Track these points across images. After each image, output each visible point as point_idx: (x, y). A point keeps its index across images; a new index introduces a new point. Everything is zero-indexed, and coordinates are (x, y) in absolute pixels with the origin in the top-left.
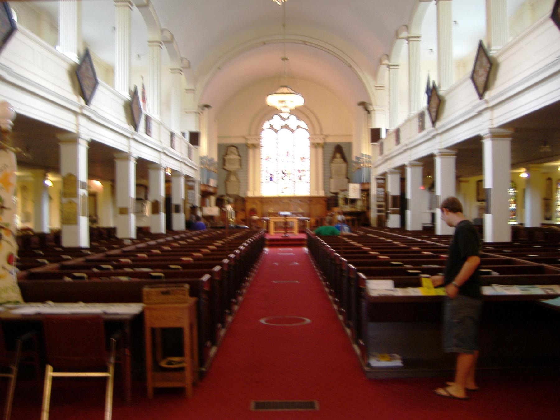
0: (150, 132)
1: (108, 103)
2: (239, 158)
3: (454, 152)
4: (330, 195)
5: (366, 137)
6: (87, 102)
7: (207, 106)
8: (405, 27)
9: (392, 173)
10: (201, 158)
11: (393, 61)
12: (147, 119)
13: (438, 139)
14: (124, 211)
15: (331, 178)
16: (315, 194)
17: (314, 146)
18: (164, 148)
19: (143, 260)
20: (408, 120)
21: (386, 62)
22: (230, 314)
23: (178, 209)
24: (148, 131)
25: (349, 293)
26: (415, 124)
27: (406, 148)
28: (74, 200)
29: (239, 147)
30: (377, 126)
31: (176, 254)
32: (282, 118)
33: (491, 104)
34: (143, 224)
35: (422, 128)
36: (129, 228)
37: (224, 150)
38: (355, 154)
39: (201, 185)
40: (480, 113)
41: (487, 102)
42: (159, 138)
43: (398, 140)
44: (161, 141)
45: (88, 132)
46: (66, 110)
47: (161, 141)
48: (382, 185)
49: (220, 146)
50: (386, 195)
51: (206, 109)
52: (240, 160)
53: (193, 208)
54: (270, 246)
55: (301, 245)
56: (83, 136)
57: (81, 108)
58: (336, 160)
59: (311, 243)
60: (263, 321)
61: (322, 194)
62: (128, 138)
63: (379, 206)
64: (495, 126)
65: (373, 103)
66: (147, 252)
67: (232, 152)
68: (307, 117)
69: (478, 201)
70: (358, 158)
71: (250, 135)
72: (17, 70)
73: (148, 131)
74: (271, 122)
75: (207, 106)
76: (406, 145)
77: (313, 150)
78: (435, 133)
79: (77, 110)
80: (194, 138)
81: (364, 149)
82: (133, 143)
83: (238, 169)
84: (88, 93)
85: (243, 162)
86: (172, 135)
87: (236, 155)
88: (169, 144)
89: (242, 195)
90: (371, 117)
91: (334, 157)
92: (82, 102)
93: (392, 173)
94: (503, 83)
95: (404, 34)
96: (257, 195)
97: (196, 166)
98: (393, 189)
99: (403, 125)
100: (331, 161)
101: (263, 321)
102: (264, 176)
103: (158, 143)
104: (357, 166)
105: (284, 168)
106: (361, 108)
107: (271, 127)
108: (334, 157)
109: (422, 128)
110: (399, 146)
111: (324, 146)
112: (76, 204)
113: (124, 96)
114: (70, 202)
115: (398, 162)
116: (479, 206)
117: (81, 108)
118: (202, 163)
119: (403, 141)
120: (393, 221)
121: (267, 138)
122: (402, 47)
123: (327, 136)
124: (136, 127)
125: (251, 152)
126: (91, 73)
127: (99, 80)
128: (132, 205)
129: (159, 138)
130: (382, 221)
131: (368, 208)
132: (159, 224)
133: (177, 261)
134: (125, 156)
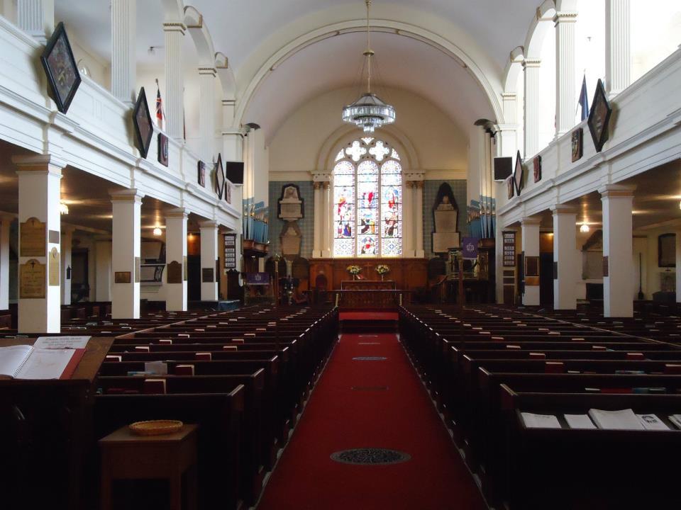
0: (166, 160)
1: (97, 112)
2: (300, 202)
3: (633, 188)
4: (432, 256)
5: (488, 170)
6: (63, 108)
7: (255, 126)
8: (521, 49)
9: (528, 223)
10: (245, 202)
11: (531, 55)
12: (161, 139)
13: (605, 169)
14: (123, 278)
15: (435, 232)
16: (411, 255)
17: (410, 185)
18: (187, 185)
19: (166, 347)
20: (556, 143)
21: (520, 58)
22: (281, 445)
23: (208, 276)
24: (162, 158)
25: (487, 424)
26: (568, 148)
27: (551, 185)
28: (40, 259)
29: (301, 187)
30: (505, 155)
31: (213, 340)
32: (363, 144)
33: (608, 158)
34: (152, 297)
35: (578, 153)
36: (131, 302)
37: (278, 190)
38: (471, 197)
39: (243, 241)
40: (598, 167)
41: (604, 155)
42: (181, 167)
43: (538, 175)
44: (183, 175)
45: (63, 154)
46: (7, 110)
47: (183, 175)
48: (513, 244)
49: (273, 185)
50: (520, 257)
51: (253, 130)
52: (302, 205)
53: (233, 275)
54: (345, 331)
55: (393, 331)
56: (139, 192)
57: (52, 115)
58: (441, 205)
59: (406, 327)
60: (335, 456)
61: (421, 254)
62: (131, 167)
63: (506, 273)
64: (561, 203)
65: (499, 120)
66: (172, 336)
67: (291, 194)
68: (401, 143)
69: (660, 265)
70: (473, 202)
71: (316, 169)
72: (84, 125)
73: (162, 158)
74: (349, 151)
75: (255, 126)
76: (552, 181)
77: (409, 191)
78: (601, 160)
79: (46, 119)
80: (235, 172)
81: (486, 189)
82: (137, 174)
83: (299, 218)
84: (64, 94)
85: (306, 208)
86: (200, 165)
87: (296, 200)
88: (196, 179)
89: (305, 255)
90: (495, 142)
91: (439, 201)
92: (138, 155)
93: (528, 223)
94: (624, 132)
95: (520, 58)
96: (325, 256)
97: (236, 212)
98: (529, 245)
99: (547, 151)
100: (434, 209)
101: (335, 456)
102: (339, 217)
103: (180, 177)
104: (474, 214)
105: (366, 213)
106: (480, 129)
107: (349, 158)
108: (439, 201)
109: (578, 153)
110: (540, 183)
111: (423, 185)
112: (44, 266)
113: (165, 139)
114: (33, 263)
115: (539, 206)
116: (661, 274)
117: (52, 115)
118: (245, 210)
119: (547, 174)
120: (531, 295)
121: (341, 176)
122: (544, 32)
123: (428, 171)
124: (144, 153)
125: (317, 193)
126: (68, 64)
127: (83, 73)
128: (135, 271)
129: (181, 167)
130: (513, 297)
131: (492, 276)
132: (179, 297)
133: (190, 358)
134: (129, 196)
